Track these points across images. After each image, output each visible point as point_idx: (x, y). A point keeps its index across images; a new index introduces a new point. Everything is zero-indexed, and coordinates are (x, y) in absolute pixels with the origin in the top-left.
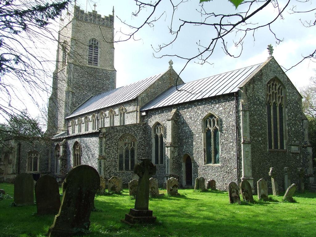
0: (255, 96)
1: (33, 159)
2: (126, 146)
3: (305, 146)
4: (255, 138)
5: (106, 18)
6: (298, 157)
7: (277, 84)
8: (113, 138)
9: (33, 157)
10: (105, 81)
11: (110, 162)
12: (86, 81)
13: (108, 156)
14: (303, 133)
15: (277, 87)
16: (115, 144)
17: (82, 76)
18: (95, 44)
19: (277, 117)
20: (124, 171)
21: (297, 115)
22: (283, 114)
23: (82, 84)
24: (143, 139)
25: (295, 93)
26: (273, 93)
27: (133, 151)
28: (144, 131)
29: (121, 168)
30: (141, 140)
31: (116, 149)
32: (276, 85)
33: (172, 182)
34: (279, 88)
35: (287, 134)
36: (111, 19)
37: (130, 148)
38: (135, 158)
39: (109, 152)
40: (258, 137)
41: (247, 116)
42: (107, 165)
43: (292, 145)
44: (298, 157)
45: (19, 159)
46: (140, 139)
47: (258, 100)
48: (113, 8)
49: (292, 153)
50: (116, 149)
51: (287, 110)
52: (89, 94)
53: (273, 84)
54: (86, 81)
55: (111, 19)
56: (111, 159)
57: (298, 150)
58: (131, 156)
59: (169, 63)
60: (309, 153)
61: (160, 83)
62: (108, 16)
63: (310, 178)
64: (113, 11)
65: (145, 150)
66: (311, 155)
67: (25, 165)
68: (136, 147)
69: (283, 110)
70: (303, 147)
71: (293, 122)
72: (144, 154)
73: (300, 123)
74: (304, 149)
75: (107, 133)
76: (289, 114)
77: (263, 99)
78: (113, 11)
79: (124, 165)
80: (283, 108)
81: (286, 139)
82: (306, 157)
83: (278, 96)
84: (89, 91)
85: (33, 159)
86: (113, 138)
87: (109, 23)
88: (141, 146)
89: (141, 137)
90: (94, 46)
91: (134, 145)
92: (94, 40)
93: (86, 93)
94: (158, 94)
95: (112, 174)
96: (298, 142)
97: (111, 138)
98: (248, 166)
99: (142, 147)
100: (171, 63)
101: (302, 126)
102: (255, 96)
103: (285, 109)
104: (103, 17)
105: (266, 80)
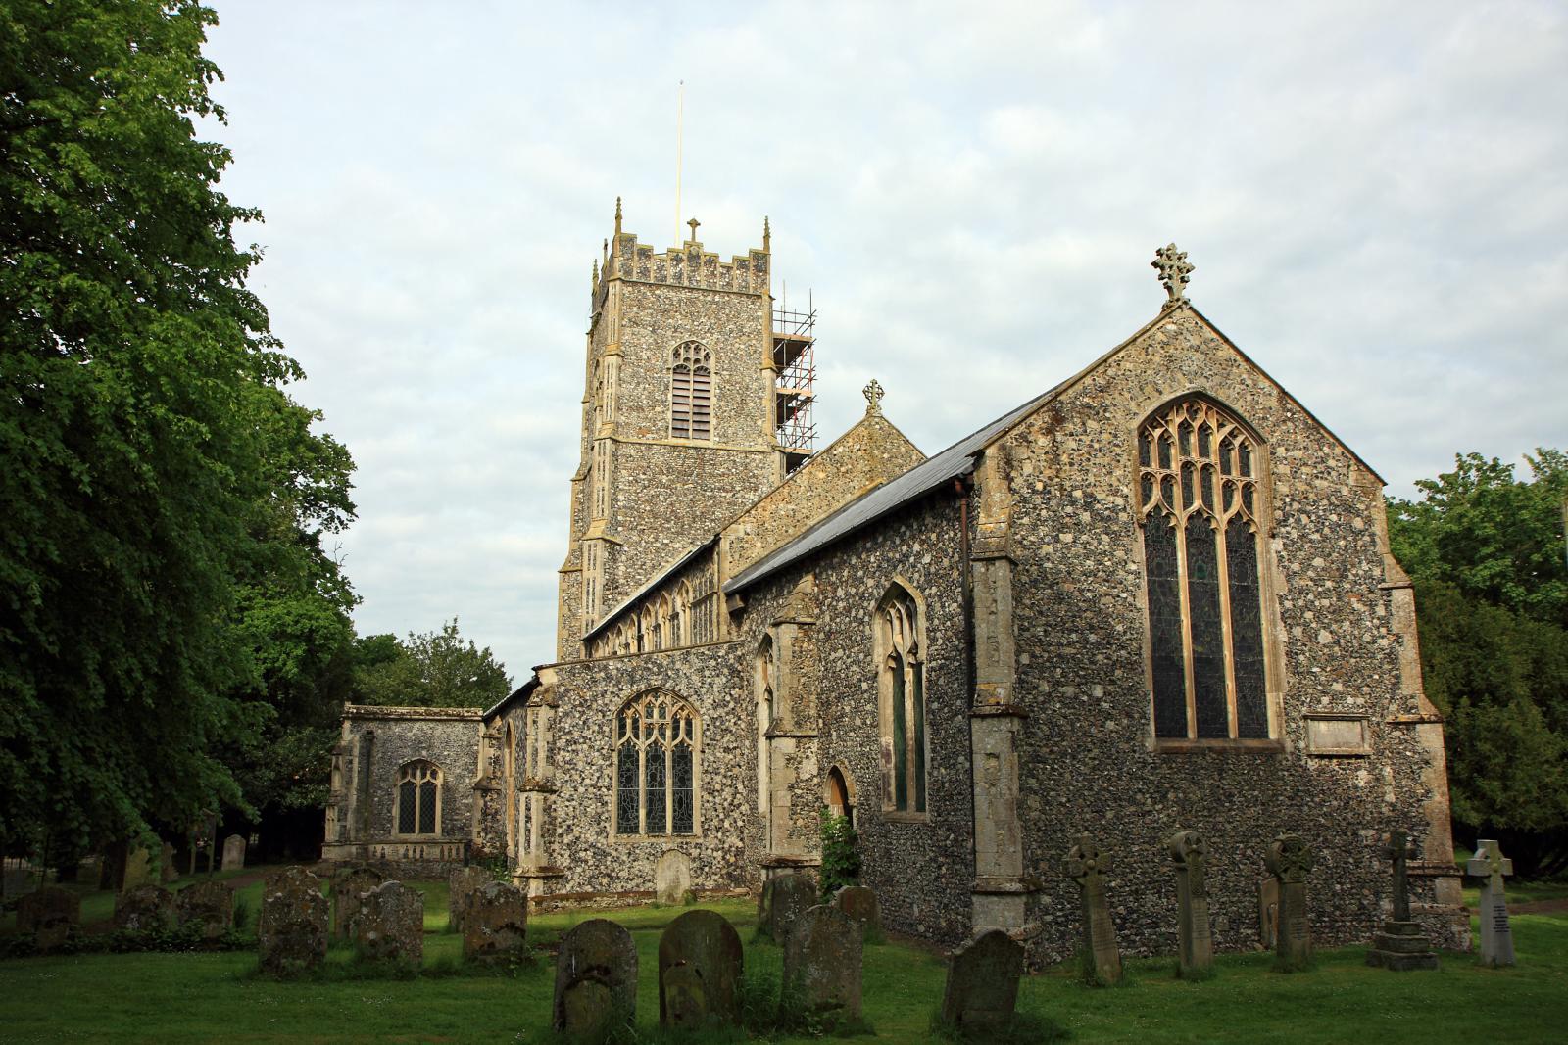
0: (1062, 488)
1: (418, 791)
2: (652, 739)
3: (1404, 717)
4: (1062, 689)
5: (742, 264)
6: (1363, 773)
7: (1213, 424)
8: (589, 707)
9: (419, 781)
10: (738, 495)
11: (574, 803)
12: (666, 499)
13: (567, 777)
14: (1392, 658)
15: (1216, 439)
16: (601, 731)
17: (649, 481)
18: (697, 361)
19: (1218, 585)
20: (642, 838)
21: (1346, 569)
22: (1260, 567)
23: (648, 508)
24: (732, 705)
25: (1331, 463)
26: (1187, 467)
27: (683, 757)
28: (734, 672)
29: (627, 824)
30: (721, 711)
31: (604, 752)
32: (1204, 430)
33: (490, 902)
34: (1225, 445)
35: (1283, 660)
36: (760, 261)
37: (668, 745)
38: (696, 784)
39: (570, 762)
40: (1087, 681)
41: (999, 583)
42: (563, 816)
43: (1313, 719)
44: (1363, 773)
45: (366, 788)
46: (716, 706)
47: (1087, 506)
48: (767, 224)
49: (1321, 757)
50: (604, 752)
51: (1277, 545)
52: (678, 545)
53: (1185, 428)
54: (666, 499)
55: (760, 261)
56: (581, 790)
57: (1363, 739)
58: (675, 775)
59: (864, 392)
60: (1426, 757)
61: (822, 475)
62: (745, 254)
63: (1437, 881)
64: (767, 237)
65: (738, 751)
66: (1440, 763)
67: (389, 811)
68: (696, 744)
69: (1259, 547)
70: (1396, 725)
71: (1326, 603)
72: (736, 770)
73: (1372, 606)
74: (1399, 733)
75: (563, 688)
76: (1296, 567)
77: (1120, 501)
78: (767, 237)
79: (642, 813)
80: (1258, 539)
81: (1278, 688)
82: (1413, 775)
83: (1218, 480)
84: (678, 533)
85: (418, 791)
86: (589, 707)
87: (751, 278)
88: (719, 738)
89: (718, 697)
90: (692, 367)
91: (689, 733)
92: (693, 346)
93: (666, 541)
94: (811, 523)
95: (586, 850)
96: (1361, 701)
97: (581, 705)
98: (996, 823)
99: (726, 740)
100: (873, 392)
101: (1385, 622)
102: (1062, 488)
103: (1267, 544)
104: (726, 259)
105: (1130, 412)
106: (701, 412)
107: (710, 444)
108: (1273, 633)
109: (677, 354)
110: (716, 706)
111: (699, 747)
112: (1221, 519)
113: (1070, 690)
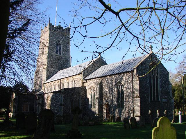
83: (155, 72)
106: (60, 51)
107: (61, 55)
108: (159, 89)
109: (57, 42)
110: (83, 95)
111: (81, 100)
112: (155, 76)
113: (143, 95)
